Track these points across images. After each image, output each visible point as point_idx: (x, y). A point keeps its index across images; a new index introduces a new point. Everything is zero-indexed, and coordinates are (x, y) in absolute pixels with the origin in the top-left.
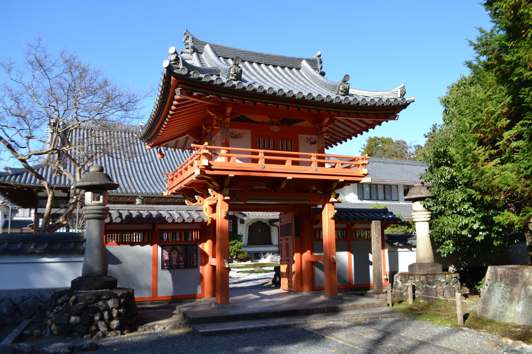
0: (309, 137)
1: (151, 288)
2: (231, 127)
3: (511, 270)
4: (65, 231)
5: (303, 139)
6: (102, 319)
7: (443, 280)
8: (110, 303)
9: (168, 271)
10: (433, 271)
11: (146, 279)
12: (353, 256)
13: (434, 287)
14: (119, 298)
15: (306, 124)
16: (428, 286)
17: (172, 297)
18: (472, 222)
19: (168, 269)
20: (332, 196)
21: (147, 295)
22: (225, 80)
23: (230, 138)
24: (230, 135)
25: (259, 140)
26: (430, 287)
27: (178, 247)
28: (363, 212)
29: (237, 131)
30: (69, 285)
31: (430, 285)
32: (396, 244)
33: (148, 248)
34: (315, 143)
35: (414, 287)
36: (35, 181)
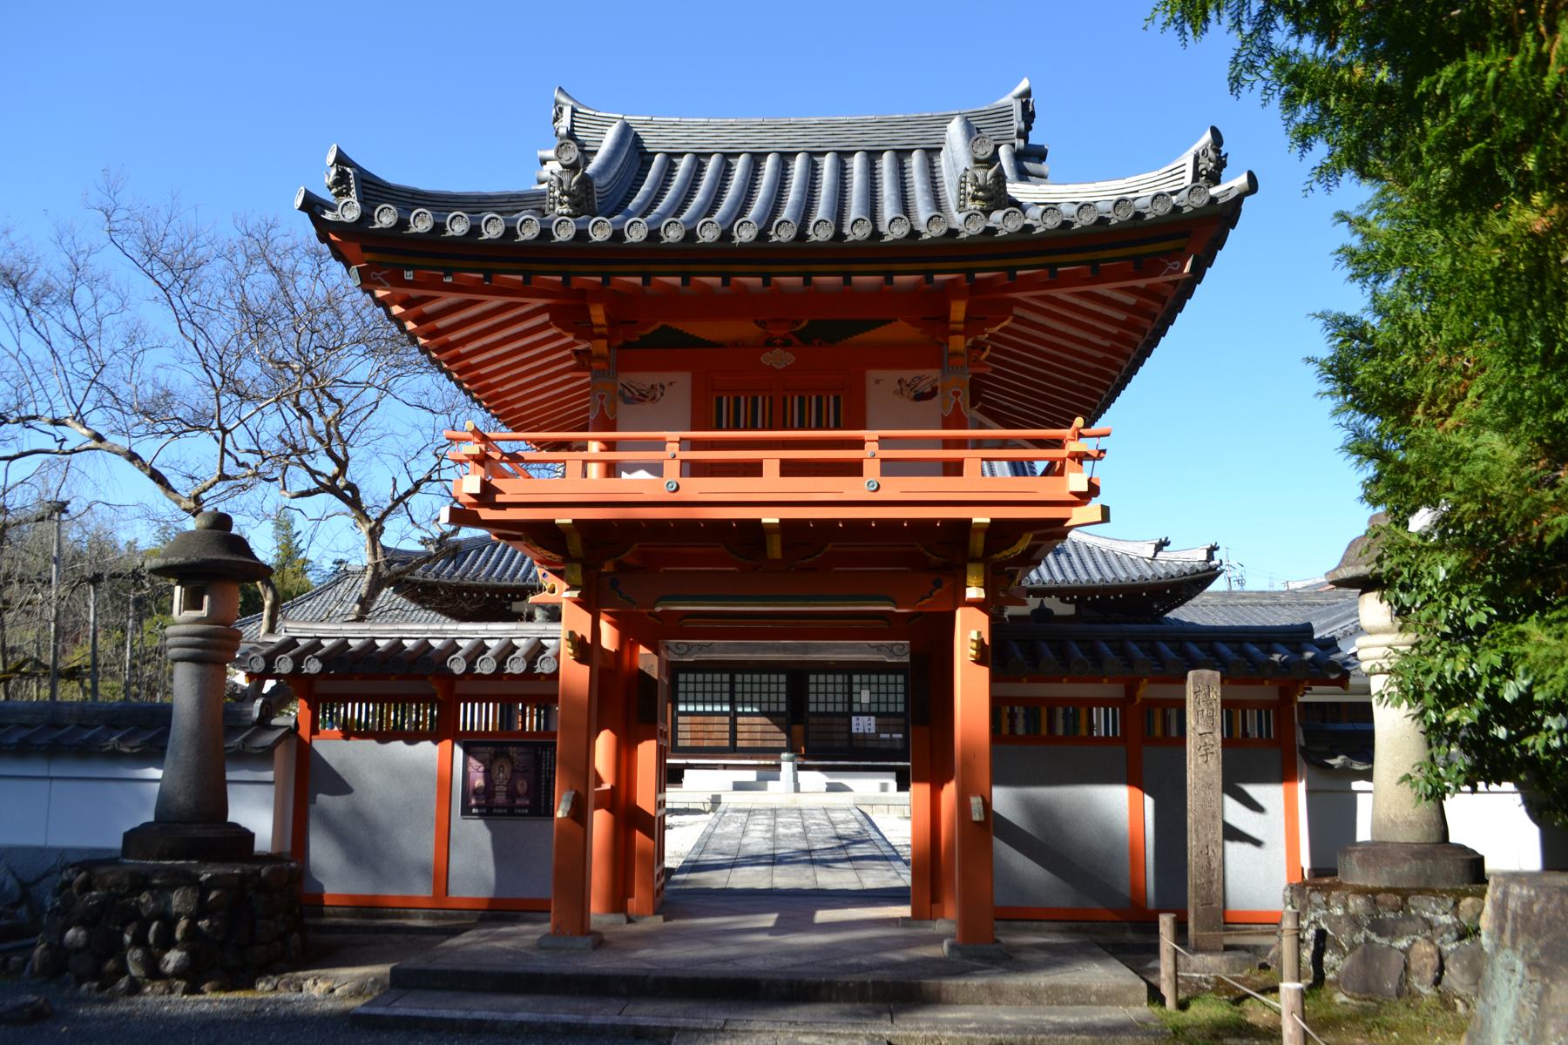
0: (908, 375)
1: (432, 871)
2: (621, 367)
3: (1556, 898)
4: (45, 693)
5: (881, 384)
6: (139, 941)
7: (1447, 919)
8: (177, 900)
9: (481, 823)
10: (1419, 876)
11: (419, 844)
12: (1149, 802)
13: (1403, 943)
14: (204, 889)
15: (900, 331)
16: (1374, 937)
17: (491, 900)
18: (1494, 672)
19: (481, 815)
20: (971, 580)
21: (421, 889)
22: (957, 219)
23: (621, 405)
24: (622, 394)
25: (720, 400)
26: (1385, 941)
27: (512, 751)
28: (1195, 641)
29: (645, 379)
30: (117, 843)
31: (1380, 935)
32: (1337, 761)
33: (427, 751)
34: (932, 394)
35: (1321, 935)
36: (1039, 573)
